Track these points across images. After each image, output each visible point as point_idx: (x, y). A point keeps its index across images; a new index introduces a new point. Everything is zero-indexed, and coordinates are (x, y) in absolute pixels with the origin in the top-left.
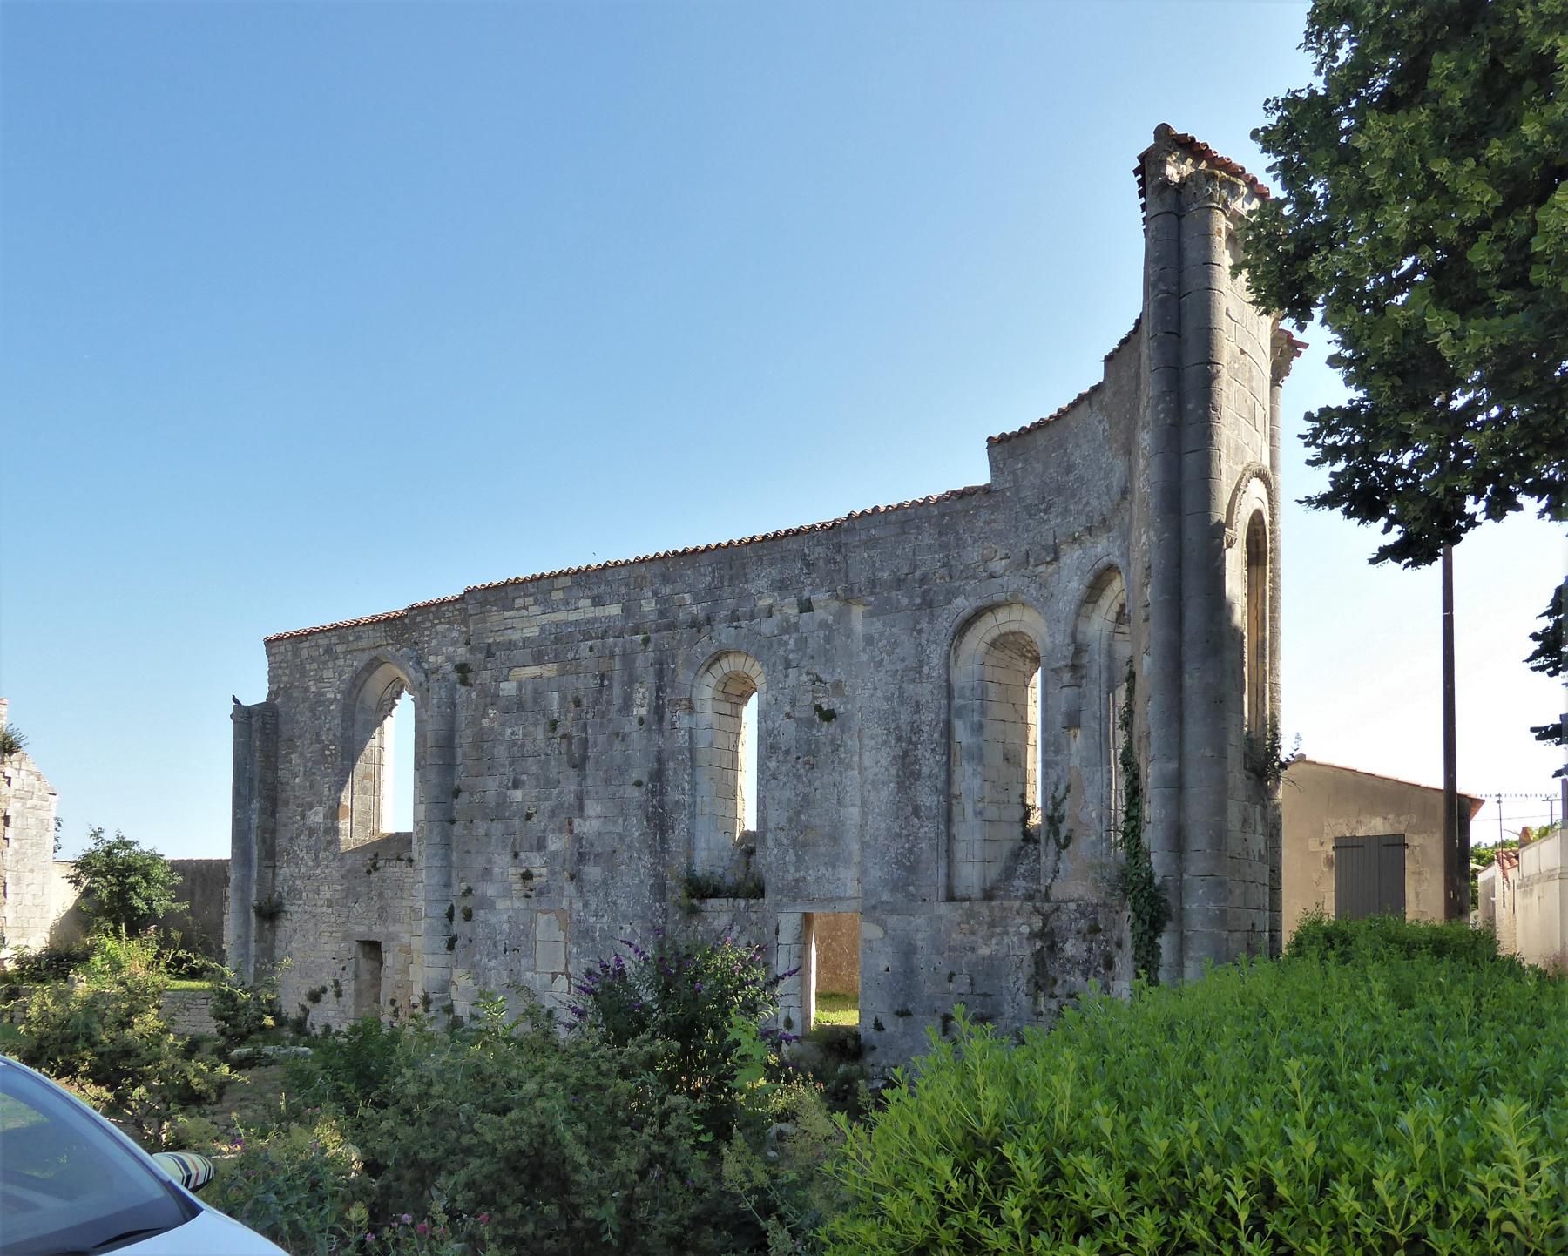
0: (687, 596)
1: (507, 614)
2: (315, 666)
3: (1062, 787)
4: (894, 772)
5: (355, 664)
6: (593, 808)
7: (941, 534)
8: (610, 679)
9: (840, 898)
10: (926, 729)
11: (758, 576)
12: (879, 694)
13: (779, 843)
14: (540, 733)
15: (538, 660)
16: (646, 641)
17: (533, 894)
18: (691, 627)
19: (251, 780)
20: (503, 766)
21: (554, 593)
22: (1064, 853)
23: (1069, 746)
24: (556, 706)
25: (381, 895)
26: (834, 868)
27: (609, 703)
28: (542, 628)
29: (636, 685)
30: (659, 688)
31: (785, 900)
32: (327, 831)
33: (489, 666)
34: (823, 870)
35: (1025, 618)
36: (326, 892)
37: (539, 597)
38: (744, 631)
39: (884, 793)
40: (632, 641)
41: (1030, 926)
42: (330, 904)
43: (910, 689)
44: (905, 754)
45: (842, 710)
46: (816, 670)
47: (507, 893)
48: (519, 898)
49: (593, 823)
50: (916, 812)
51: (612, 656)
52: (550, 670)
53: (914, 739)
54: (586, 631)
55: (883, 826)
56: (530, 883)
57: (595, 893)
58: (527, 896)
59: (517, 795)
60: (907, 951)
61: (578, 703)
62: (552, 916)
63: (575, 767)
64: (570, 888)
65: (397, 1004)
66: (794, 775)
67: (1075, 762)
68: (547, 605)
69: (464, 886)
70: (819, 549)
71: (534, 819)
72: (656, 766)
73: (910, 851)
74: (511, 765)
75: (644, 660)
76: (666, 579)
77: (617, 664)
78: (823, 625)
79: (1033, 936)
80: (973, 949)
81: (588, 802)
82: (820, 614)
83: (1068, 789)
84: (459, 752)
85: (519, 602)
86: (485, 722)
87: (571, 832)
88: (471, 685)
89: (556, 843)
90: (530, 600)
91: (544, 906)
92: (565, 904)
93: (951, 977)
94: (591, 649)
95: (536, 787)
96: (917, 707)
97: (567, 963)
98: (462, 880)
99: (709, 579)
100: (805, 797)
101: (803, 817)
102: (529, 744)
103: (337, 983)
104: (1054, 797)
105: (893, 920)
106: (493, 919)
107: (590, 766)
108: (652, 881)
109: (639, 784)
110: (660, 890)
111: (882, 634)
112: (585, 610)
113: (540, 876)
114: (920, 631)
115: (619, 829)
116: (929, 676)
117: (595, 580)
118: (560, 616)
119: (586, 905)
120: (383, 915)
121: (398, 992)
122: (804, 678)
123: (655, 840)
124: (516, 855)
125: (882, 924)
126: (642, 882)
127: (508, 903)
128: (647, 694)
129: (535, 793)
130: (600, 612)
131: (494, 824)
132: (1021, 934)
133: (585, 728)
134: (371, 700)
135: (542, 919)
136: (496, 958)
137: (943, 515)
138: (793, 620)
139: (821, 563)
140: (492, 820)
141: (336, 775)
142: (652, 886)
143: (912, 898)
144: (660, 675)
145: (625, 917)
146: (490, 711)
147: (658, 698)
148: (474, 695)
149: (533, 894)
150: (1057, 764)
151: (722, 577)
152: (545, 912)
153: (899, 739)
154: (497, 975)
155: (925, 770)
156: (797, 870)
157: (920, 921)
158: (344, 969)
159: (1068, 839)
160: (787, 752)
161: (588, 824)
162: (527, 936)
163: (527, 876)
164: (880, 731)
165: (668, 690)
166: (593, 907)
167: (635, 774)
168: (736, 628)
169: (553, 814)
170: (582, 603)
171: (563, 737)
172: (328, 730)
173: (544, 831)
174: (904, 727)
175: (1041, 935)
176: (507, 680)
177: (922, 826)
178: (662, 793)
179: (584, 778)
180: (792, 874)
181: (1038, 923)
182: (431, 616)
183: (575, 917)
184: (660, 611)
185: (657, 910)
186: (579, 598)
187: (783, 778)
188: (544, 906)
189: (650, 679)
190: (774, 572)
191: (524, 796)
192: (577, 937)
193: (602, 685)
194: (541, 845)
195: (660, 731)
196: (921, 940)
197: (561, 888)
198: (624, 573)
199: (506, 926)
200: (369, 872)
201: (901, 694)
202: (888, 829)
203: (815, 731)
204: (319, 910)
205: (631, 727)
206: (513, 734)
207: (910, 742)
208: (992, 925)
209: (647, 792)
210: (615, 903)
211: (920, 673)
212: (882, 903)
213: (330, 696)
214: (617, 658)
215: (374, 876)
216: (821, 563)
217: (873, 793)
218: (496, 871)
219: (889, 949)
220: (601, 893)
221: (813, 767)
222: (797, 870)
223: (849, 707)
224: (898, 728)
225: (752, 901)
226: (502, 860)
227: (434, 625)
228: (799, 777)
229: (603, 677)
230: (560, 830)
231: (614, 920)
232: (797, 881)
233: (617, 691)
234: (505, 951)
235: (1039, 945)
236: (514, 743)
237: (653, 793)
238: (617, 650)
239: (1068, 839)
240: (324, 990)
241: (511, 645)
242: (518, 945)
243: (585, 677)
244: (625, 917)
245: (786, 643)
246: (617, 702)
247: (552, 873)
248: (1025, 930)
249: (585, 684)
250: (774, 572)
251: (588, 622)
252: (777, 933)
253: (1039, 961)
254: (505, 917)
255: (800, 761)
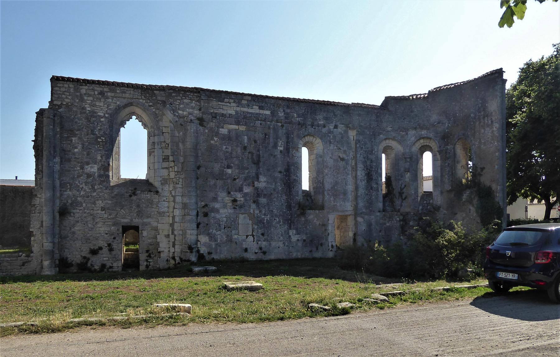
0: (295, 114)
1: (220, 103)
2: (91, 98)
3: (403, 186)
4: (366, 177)
5: (118, 103)
6: (262, 179)
7: (377, 118)
8: (269, 136)
9: (346, 211)
10: (374, 167)
11: (319, 114)
12: (362, 156)
13: (328, 194)
14: (239, 150)
15: (238, 123)
16: (282, 126)
17: (237, 207)
18: (299, 125)
19: (54, 147)
20: (222, 159)
21: (243, 101)
22: (404, 201)
23: (405, 176)
24: (246, 141)
25: (138, 206)
26: (345, 202)
27: (268, 144)
28: (237, 112)
29: (279, 140)
30: (288, 142)
31: (330, 211)
32: (100, 176)
33: (214, 121)
34: (342, 203)
35: (393, 143)
36: (100, 203)
37: (236, 100)
38: (317, 130)
39: (363, 183)
40: (277, 125)
41: (399, 218)
42: (103, 209)
43: (370, 156)
44: (369, 173)
45: (346, 158)
46: (339, 146)
47: (225, 207)
48: (231, 209)
49: (263, 184)
50: (372, 188)
51: (269, 128)
52: (242, 128)
53: (371, 169)
54: (257, 117)
55: (363, 191)
56: (236, 204)
57: (264, 207)
58: (234, 208)
59: (229, 171)
60: (369, 225)
61: (255, 142)
62: (246, 215)
63: (254, 164)
64: (254, 206)
65: (150, 252)
66: (333, 175)
67: (407, 180)
68: (239, 104)
69: (203, 203)
70: (338, 111)
71: (237, 181)
72: (287, 167)
73: (370, 199)
74: (226, 160)
75: (281, 132)
76: (288, 107)
77: (272, 131)
78: (341, 133)
79: (400, 221)
80: (385, 224)
81: (261, 176)
82: (339, 130)
83: (405, 186)
84: (200, 152)
85: (226, 100)
86: (212, 142)
87: (254, 186)
88: (205, 127)
89: (247, 190)
90: (232, 101)
91: (243, 211)
92: (252, 211)
93: (380, 231)
94: (261, 124)
95: (238, 169)
96: (372, 161)
97: (253, 231)
98: (202, 201)
99: (303, 111)
100: (336, 182)
101: (336, 188)
102: (234, 153)
103: (109, 245)
104: (401, 187)
105: (366, 217)
106: (218, 216)
107: (261, 164)
108: (286, 204)
109: (280, 172)
110: (289, 207)
111: (362, 140)
112: (255, 110)
113: (241, 201)
114: (372, 141)
115: (273, 187)
116: (374, 154)
117: (261, 101)
118: (245, 110)
119: (260, 212)
120: (140, 214)
121: (151, 247)
122: (335, 147)
123: (287, 190)
124: (229, 193)
125: (363, 218)
126: (282, 204)
127: (226, 210)
128: (283, 143)
129: (237, 171)
130: (261, 112)
131: (218, 181)
132: (397, 220)
133: (259, 151)
134: (119, 120)
135: (241, 216)
136: (220, 231)
137: (378, 113)
138: (332, 130)
139: (339, 115)
140: (217, 179)
141: (106, 151)
142: (286, 206)
143: (371, 211)
144: (288, 138)
145: (276, 216)
146: (215, 138)
147: (287, 145)
148: (207, 131)
149: (237, 207)
150: (401, 180)
151: (308, 112)
152: (242, 214)
153: (367, 169)
154: (221, 236)
155: (374, 178)
156: (334, 202)
157: (373, 217)
158: (114, 238)
159: (405, 198)
160: (331, 168)
161: (261, 184)
162: (235, 222)
163: (235, 201)
164: (362, 166)
165: (291, 143)
166: (264, 212)
167: (279, 169)
168: (314, 128)
169: (245, 179)
170: (254, 107)
171: (249, 153)
172: (100, 129)
173: (242, 185)
174: (368, 166)
175: (403, 220)
176: (223, 128)
177: (373, 193)
178: (289, 176)
179: (259, 168)
180: (332, 203)
181: (402, 218)
182: (181, 95)
183: (256, 215)
184: (285, 117)
185: (288, 213)
186: (254, 105)
187: (329, 176)
188: (243, 211)
189: (284, 139)
190: (325, 115)
191: (232, 171)
192: (257, 223)
193: (265, 137)
194: (240, 190)
195: (288, 156)
196: (373, 221)
197: (250, 206)
198: (273, 101)
199: (225, 219)
200: (130, 196)
201: (368, 157)
202: (365, 192)
203: (338, 163)
204: (95, 212)
205: (277, 153)
206: (226, 148)
207: (370, 170)
208: (390, 218)
209: (284, 175)
210: (272, 211)
211: (372, 152)
212: (363, 212)
213: (101, 114)
214: (271, 129)
215: (134, 198)
216: (339, 115)
217: (361, 183)
218: (219, 199)
219: (365, 225)
220: (267, 208)
221: (338, 173)
222: (334, 202)
223: (348, 158)
224: (367, 166)
225: (321, 211)
226: (222, 195)
227: (182, 99)
228: (334, 176)
229: (266, 135)
230: (249, 185)
231: (272, 217)
232: (334, 205)
233: (271, 140)
234: (225, 228)
235: (402, 223)
236: (227, 152)
237: (286, 175)
238: (271, 126)
239: (405, 198)
240: (101, 248)
241: (223, 115)
242: (231, 225)
243: (259, 133)
244: (276, 216)
245: (330, 137)
246: (271, 145)
247: (246, 200)
248: (398, 219)
249: (259, 136)
250: (325, 115)
251: (257, 114)
252: (328, 220)
253: (402, 227)
254: (224, 216)
255: (334, 171)
